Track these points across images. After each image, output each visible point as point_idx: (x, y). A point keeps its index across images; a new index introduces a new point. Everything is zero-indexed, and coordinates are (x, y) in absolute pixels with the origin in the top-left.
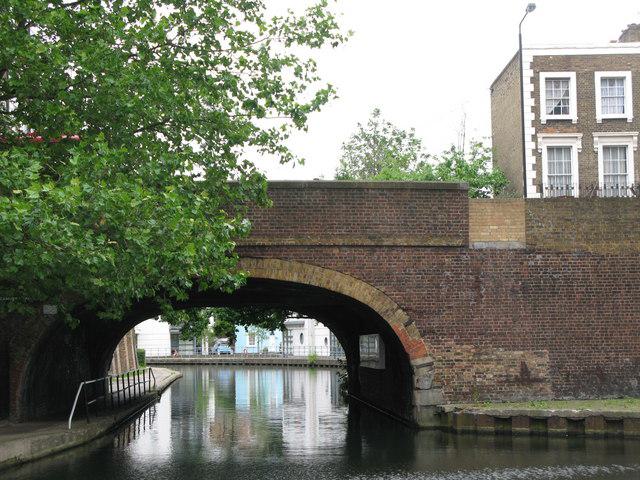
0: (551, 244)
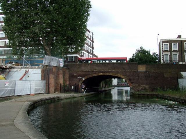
0: (149, 71)
